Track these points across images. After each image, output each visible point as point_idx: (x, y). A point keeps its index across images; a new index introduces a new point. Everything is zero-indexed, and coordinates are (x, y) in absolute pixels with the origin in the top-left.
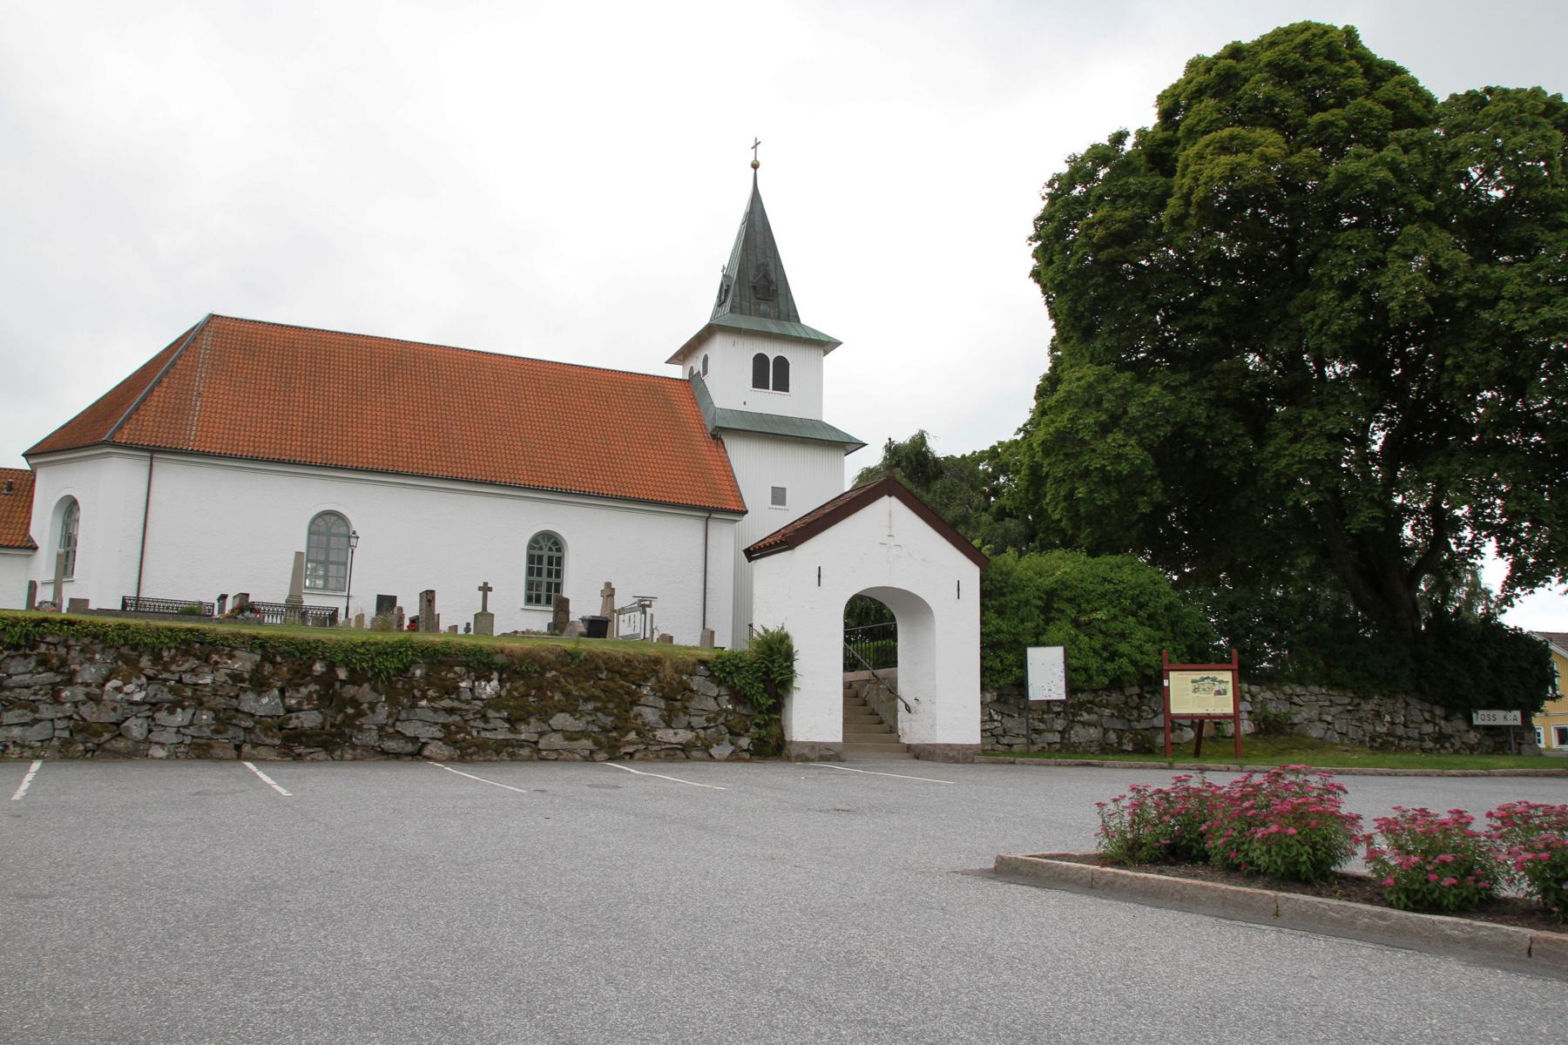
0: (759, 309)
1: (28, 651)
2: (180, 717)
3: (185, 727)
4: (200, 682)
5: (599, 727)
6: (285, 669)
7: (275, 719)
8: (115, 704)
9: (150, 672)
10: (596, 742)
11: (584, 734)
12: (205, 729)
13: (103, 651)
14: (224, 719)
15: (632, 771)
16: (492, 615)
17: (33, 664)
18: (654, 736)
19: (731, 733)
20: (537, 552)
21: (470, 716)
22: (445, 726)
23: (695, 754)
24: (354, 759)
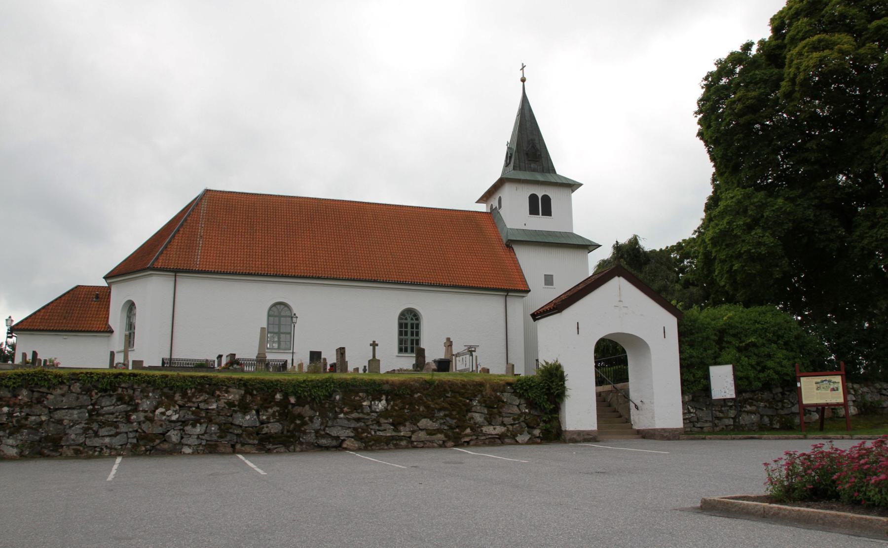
1: (111, 393)
2: (199, 429)
3: (202, 435)
4: (210, 408)
5: (448, 426)
7: (254, 428)
8: (162, 422)
9: (180, 402)
10: (446, 436)
11: (438, 431)
12: (214, 435)
13: (153, 392)
15: (469, 452)
16: (379, 360)
18: (482, 430)
19: (528, 427)
20: (404, 321)
21: (370, 423)
22: (355, 429)
23: (507, 440)
24: (302, 451)
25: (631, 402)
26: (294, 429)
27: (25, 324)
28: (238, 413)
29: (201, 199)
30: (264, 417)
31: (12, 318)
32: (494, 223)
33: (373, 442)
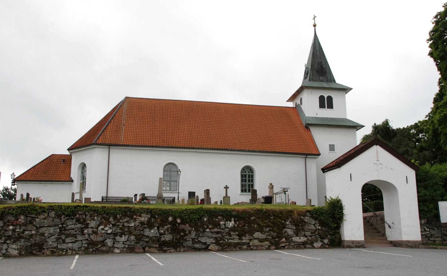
0: (320, 79)
1: (73, 217)
2: (124, 238)
3: (126, 242)
4: (130, 225)
5: (271, 237)
7: (156, 238)
8: (102, 234)
9: (113, 223)
10: (270, 243)
11: (266, 240)
12: (132, 242)
13: (97, 216)
14: (139, 238)
15: (285, 253)
17: (75, 221)
18: (292, 240)
19: (321, 238)
20: (244, 173)
22: (216, 238)
24: (184, 251)
25: (385, 223)
26: (180, 238)
30: (162, 231)
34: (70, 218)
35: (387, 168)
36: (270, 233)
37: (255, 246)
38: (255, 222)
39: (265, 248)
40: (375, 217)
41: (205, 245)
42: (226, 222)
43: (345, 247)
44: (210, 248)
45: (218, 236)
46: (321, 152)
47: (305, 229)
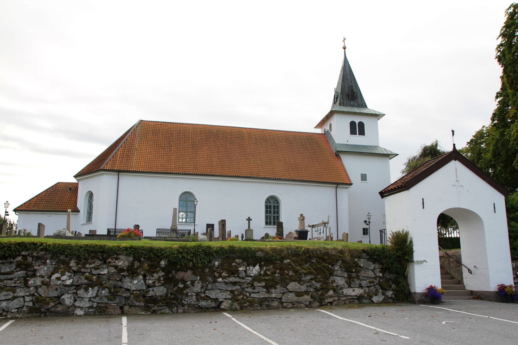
0: (350, 104)
1: (12, 260)
2: (92, 293)
3: (93, 298)
4: (101, 273)
5: (314, 289)
6: (146, 264)
7: (141, 291)
8: (57, 287)
9: (75, 269)
10: (312, 297)
11: (307, 293)
12: (104, 298)
13: (51, 258)
14: (113, 295)
15: (337, 317)
16: (252, 230)
17: (14, 267)
18: (343, 292)
19: (382, 288)
20: (269, 204)
21: (245, 286)
22: (232, 292)
23: (364, 301)
24: (184, 312)
25: (463, 267)
26: (176, 291)
27: (23, 206)
28: (127, 278)
29: (137, 126)
30: (150, 282)
31: (9, 202)
32: (327, 140)
33: (248, 303)
34: (7, 261)
35: (469, 191)
36: (312, 283)
37: (290, 302)
38: (290, 267)
39: (305, 305)
40: (447, 258)
41: (215, 302)
42: (248, 268)
43: (417, 302)
44: (222, 307)
45: (235, 288)
46: (352, 182)
47: (361, 277)
